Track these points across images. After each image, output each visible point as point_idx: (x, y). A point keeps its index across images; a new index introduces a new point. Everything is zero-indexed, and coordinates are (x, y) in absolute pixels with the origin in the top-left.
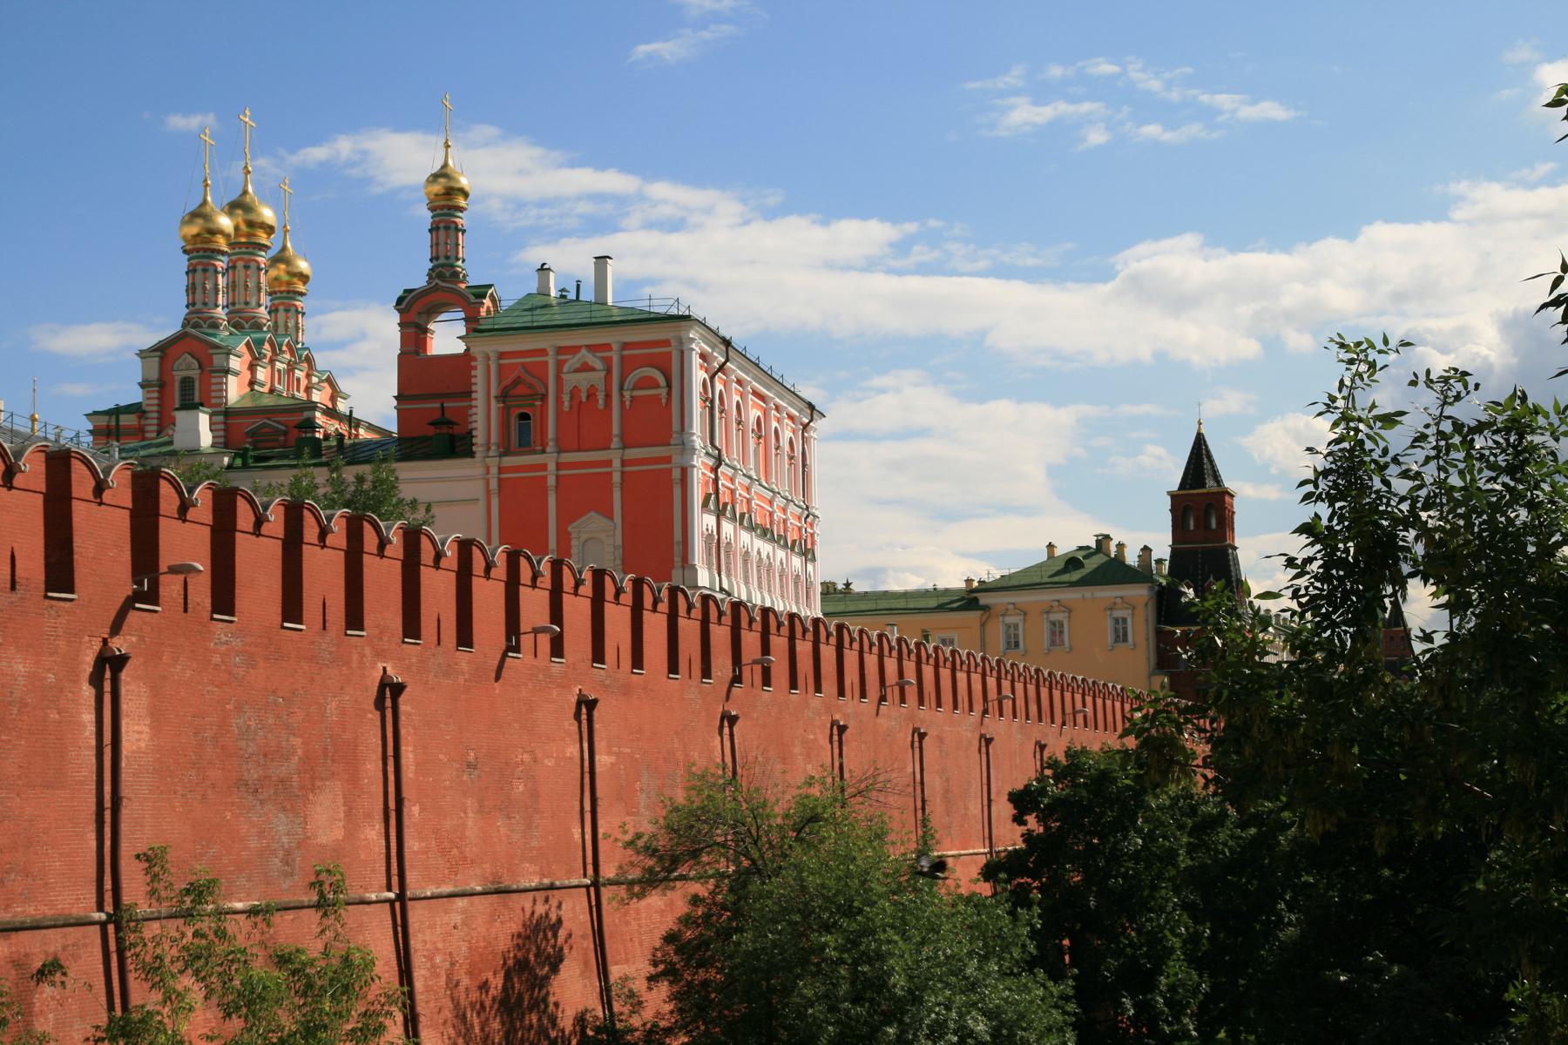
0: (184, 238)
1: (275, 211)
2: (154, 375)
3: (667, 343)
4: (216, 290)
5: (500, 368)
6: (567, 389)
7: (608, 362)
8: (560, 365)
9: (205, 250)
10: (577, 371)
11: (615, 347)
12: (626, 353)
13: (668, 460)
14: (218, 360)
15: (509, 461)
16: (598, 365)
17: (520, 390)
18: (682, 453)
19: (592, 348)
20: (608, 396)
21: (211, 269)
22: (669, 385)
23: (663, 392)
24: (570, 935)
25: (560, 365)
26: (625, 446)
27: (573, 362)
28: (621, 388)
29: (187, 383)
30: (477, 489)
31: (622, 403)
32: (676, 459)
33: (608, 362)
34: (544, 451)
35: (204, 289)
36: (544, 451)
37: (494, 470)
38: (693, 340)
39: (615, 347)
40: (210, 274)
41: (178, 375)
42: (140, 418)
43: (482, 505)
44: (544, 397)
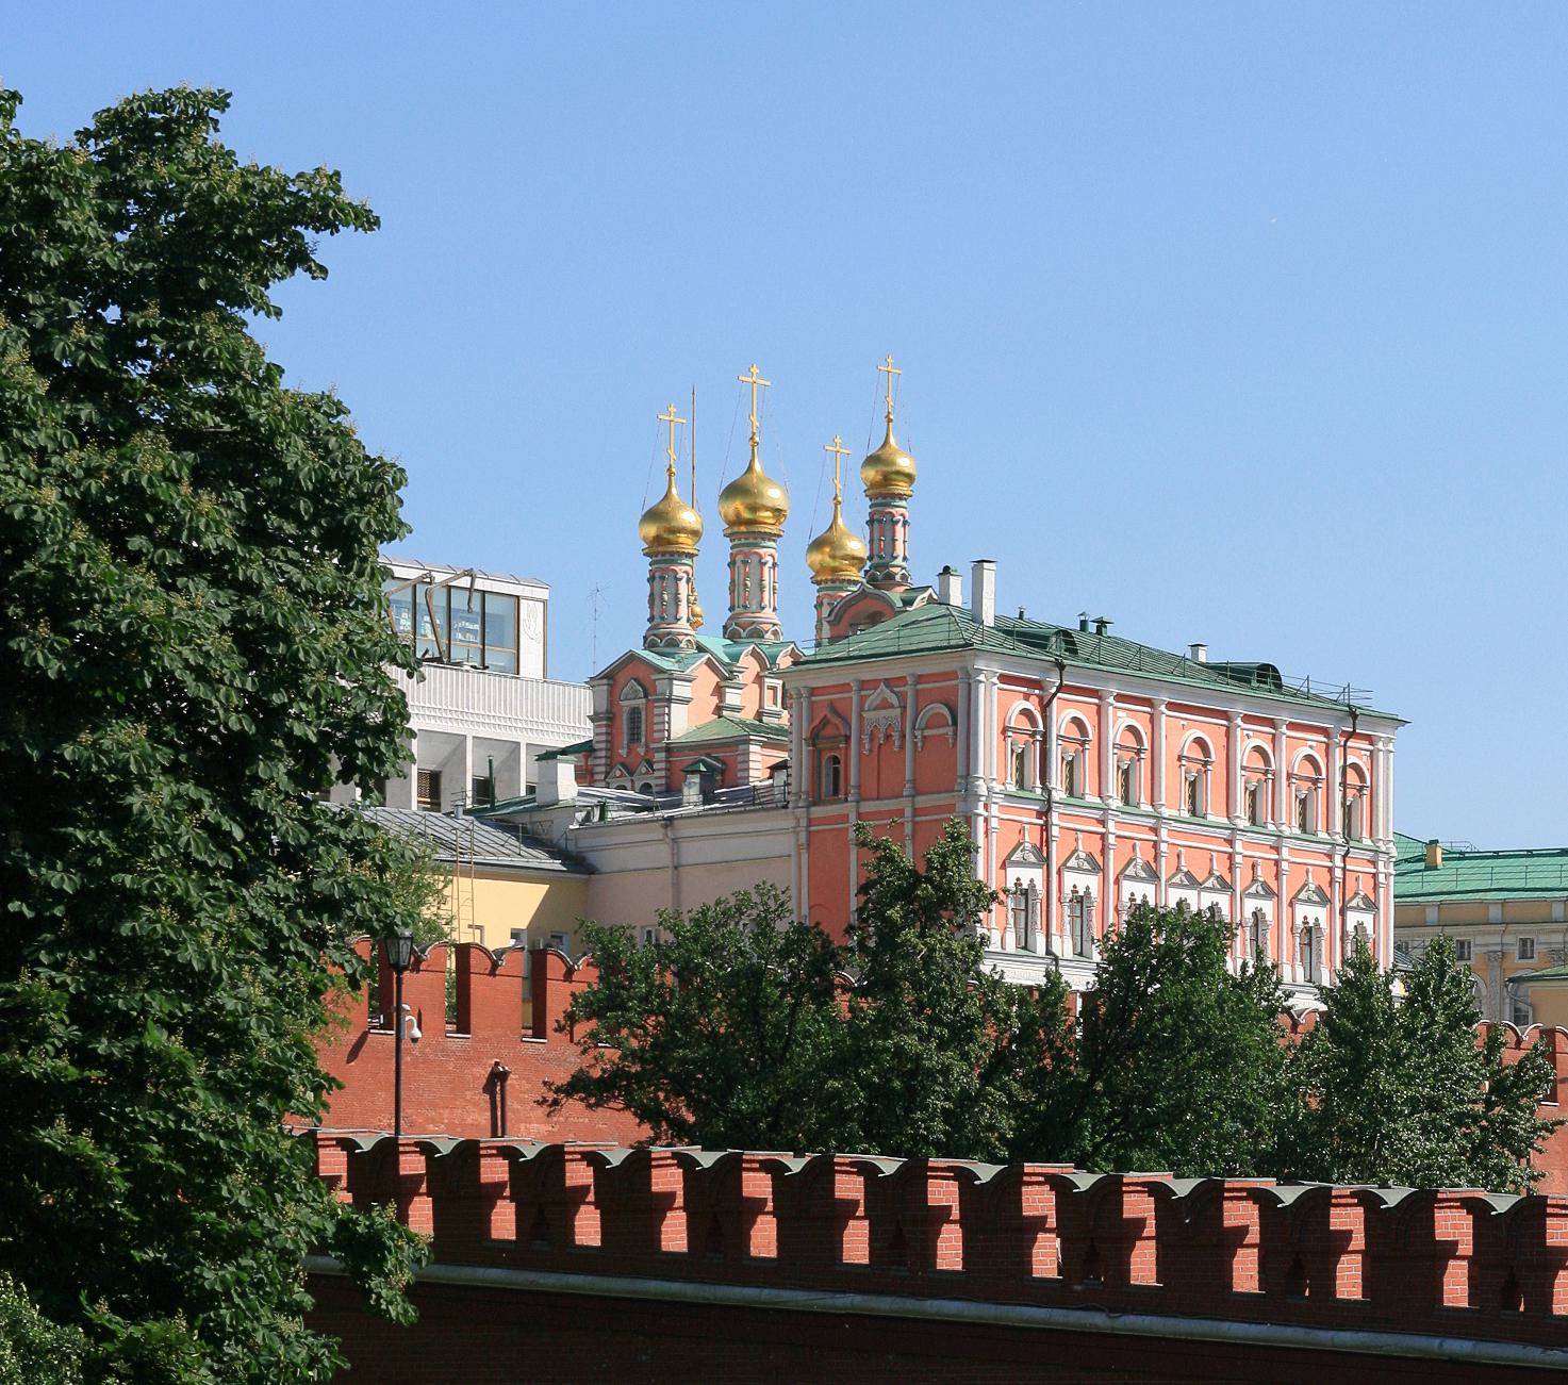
0: (645, 539)
1: (786, 491)
2: (603, 707)
3: (951, 675)
4: (677, 601)
5: (812, 705)
6: (868, 729)
7: (901, 697)
8: (862, 700)
9: (663, 554)
10: (877, 708)
11: (910, 680)
12: (920, 687)
13: (951, 808)
14: (661, 686)
15: (817, 811)
16: (895, 702)
17: (829, 731)
18: (965, 800)
19: (888, 682)
20: (903, 736)
21: (755, 559)
22: (955, 723)
23: (949, 730)
24: (1544, 1139)
25: (862, 700)
26: (917, 792)
27: (873, 698)
28: (914, 728)
29: (635, 713)
30: (784, 844)
31: (860, 754)
32: (960, 807)
33: (901, 697)
34: (846, 800)
35: (662, 599)
36: (846, 800)
37: (804, 822)
38: (980, 671)
39: (910, 680)
40: (752, 568)
41: (626, 705)
42: (587, 757)
43: (794, 859)
44: (848, 739)
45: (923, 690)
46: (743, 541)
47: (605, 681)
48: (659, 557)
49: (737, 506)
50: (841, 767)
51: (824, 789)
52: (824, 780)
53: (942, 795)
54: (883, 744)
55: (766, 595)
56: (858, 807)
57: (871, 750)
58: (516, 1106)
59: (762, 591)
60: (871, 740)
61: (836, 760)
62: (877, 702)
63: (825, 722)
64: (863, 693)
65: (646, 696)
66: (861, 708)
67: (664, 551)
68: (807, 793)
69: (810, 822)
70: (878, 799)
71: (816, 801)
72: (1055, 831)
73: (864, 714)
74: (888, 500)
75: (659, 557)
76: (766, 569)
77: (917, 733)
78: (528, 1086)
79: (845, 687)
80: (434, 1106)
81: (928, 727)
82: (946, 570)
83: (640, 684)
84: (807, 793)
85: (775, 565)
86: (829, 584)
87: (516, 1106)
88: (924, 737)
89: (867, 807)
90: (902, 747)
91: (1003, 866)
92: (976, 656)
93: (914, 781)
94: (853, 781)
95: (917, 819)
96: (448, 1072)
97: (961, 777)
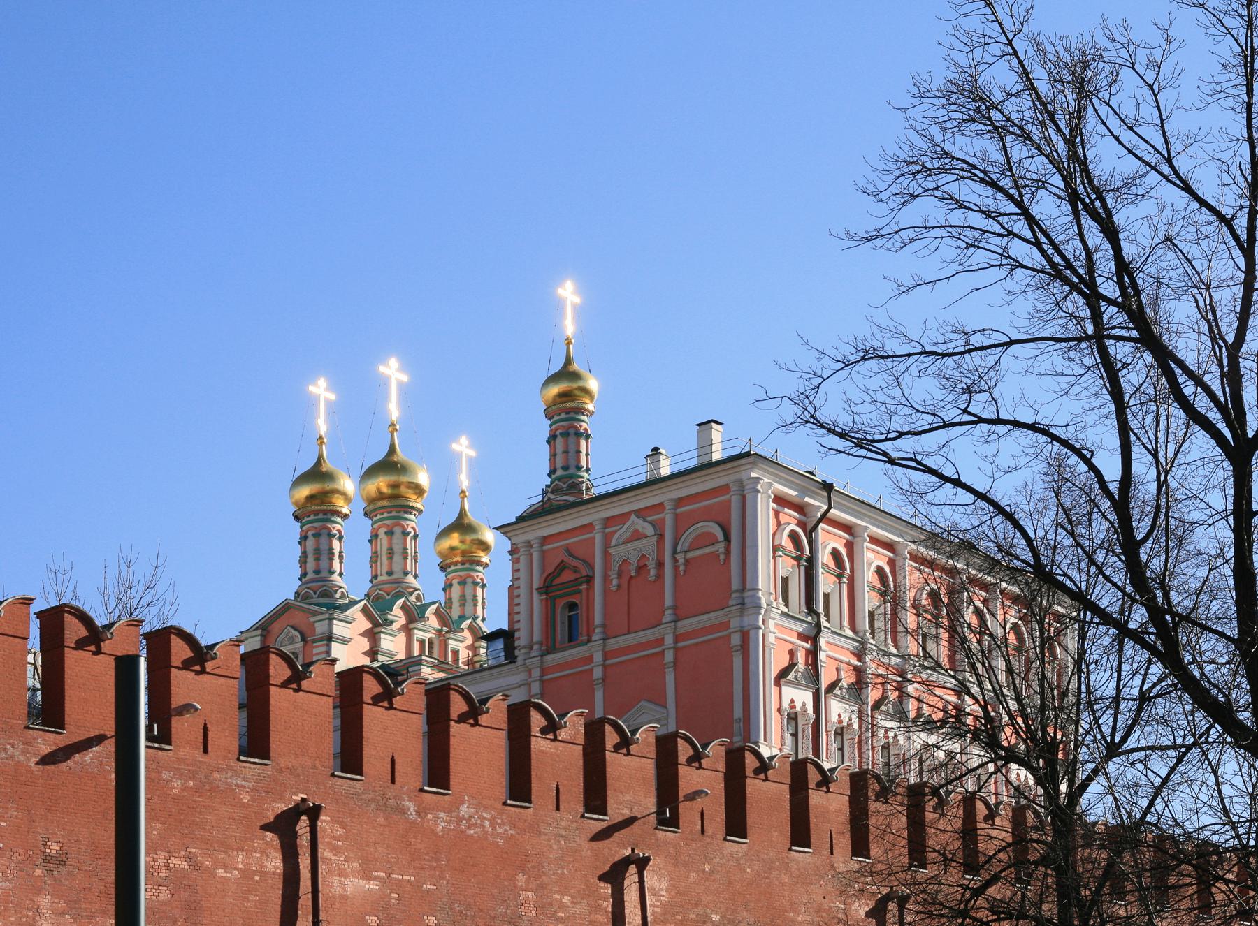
3: (725, 489)
5: (544, 555)
8: (607, 539)
9: (316, 513)
11: (668, 506)
16: (650, 530)
17: (567, 576)
19: (640, 513)
20: (660, 565)
22: (727, 538)
23: (721, 547)
27: (622, 532)
28: (674, 552)
31: (606, 592)
34: (589, 641)
37: (536, 673)
39: (668, 506)
44: (590, 580)
45: (682, 513)
46: (386, 515)
47: (259, 632)
48: (312, 517)
49: (381, 483)
50: (581, 612)
51: (559, 637)
52: (559, 628)
53: (712, 614)
54: (636, 577)
55: (409, 561)
56: (604, 646)
57: (619, 586)
58: (327, 854)
59: (405, 558)
60: (620, 576)
61: (572, 606)
62: (628, 535)
63: (562, 567)
64: (608, 530)
65: (303, 639)
66: (607, 545)
67: (316, 514)
68: (541, 643)
69: (544, 671)
70: (629, 633)
71: (550, 647)
72: (822, 656)
73: (611, 551)
74: (572, 415)
75: (312, 517)
76: (409, 539)
77: (678, 557)
78: (341, 831)
79: (589, 527)
80: (227, 847)
81: (691, 549)
82: (656, 450)
83: (295, 629)
84: (541, 643)
85: (416, 536)
86: (459, 566)
87: (327, 854)
88: (687, 562)
89: (614, 644)
90: (660, 576)
91: (778, 682)
92: (753, 463)
93: (675, 608)
94: (598, 619)
95: (680, 645)
96: (243, 806)
97: (736, 591)
